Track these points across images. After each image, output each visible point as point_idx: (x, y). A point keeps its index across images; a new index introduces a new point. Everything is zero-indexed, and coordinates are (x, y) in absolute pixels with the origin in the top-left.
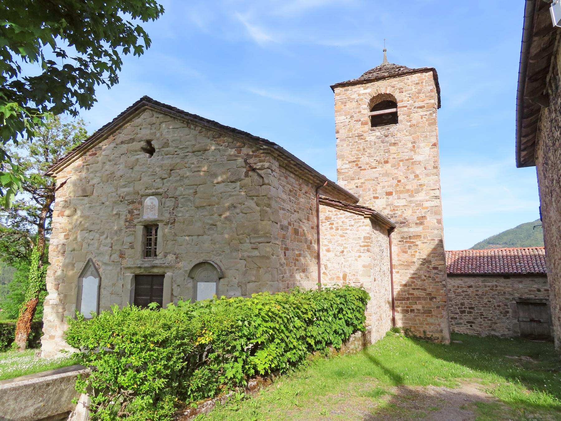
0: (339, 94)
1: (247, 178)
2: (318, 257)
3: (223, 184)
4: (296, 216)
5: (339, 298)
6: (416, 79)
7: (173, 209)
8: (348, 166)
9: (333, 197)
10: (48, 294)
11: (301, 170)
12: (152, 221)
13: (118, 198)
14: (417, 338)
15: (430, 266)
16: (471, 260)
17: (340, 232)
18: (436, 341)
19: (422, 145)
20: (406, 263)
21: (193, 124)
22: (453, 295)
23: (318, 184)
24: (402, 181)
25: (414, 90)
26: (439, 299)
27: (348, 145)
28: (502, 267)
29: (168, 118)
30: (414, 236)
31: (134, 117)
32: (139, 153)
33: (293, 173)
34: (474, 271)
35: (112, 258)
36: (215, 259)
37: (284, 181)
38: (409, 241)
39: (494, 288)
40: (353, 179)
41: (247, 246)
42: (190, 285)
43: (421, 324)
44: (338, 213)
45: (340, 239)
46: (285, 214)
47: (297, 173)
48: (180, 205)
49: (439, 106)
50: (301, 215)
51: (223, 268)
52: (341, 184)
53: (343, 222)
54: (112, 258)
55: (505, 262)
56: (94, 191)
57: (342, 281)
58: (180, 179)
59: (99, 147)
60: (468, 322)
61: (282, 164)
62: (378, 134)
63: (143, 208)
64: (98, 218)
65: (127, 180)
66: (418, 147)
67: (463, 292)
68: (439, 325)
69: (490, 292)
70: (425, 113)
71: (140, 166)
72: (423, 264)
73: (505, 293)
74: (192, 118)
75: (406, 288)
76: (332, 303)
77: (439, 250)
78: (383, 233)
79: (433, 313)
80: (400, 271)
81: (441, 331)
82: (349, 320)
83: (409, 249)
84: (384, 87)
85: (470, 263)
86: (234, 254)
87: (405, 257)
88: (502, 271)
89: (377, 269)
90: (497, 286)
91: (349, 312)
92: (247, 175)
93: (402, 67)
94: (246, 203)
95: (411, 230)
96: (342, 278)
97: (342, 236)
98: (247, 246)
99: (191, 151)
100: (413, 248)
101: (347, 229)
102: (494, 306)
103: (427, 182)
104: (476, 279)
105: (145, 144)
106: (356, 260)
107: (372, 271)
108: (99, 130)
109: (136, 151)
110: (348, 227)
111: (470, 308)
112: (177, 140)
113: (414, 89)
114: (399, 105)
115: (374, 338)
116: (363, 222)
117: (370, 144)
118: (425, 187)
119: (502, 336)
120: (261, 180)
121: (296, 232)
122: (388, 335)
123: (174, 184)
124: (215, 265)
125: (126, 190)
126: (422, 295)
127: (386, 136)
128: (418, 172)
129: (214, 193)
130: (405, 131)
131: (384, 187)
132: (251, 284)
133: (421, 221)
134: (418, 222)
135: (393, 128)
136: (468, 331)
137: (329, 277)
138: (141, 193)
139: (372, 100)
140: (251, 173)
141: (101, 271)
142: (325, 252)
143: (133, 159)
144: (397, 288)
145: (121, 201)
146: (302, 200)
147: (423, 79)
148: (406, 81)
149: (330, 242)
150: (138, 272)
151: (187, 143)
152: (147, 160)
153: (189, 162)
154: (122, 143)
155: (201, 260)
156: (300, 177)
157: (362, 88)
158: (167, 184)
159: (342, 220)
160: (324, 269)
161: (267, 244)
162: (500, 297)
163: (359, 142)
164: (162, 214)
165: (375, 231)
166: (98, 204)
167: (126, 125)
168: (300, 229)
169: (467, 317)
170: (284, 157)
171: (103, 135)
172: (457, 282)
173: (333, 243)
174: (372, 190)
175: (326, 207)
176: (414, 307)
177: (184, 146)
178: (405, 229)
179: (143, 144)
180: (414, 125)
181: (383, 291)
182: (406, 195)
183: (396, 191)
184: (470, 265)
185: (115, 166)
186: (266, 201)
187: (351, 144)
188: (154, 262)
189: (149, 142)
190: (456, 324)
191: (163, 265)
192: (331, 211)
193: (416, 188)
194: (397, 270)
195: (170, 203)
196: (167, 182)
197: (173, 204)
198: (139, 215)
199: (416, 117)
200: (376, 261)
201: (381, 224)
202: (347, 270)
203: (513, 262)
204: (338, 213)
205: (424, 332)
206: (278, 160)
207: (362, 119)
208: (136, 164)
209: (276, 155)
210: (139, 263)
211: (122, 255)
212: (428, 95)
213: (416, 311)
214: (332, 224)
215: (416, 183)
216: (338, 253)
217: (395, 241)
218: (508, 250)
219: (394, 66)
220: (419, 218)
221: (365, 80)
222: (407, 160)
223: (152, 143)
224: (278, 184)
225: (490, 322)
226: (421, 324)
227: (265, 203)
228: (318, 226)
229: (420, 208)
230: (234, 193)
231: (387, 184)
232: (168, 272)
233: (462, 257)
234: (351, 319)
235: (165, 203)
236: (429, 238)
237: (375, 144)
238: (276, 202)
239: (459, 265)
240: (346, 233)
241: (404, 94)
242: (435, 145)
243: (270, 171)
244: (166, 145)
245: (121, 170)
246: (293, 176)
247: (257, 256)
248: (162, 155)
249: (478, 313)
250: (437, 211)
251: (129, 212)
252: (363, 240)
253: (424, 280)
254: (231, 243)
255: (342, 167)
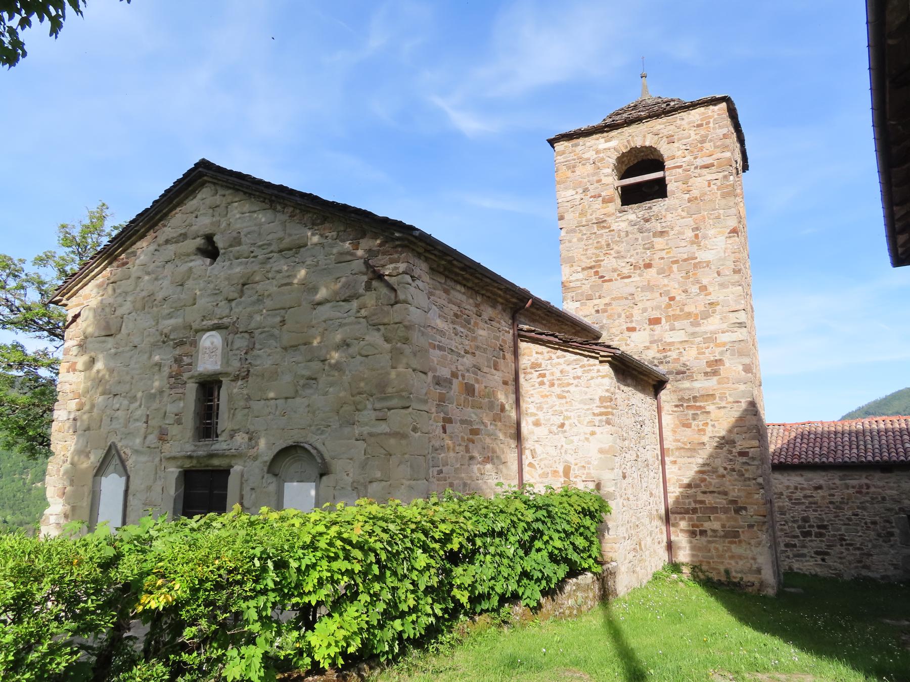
0: (563, 153)
1: (368, 293)
2: (518, 436)
3: (328, 305)
4: (468, 360)
5: (533, 510)
6: (698, 117)
7: (246, 353)
8: (580, 276)
9: (550, 329)
10: (48, 505)
11: (477, 278)
12: (210, 376)
13: (159, 338)
14: (713, 583)
15: (734, 450)
16: (818, 440)
17: (557, 390)
18: (750, 589)
19: (711, 232)
20: (689, 446)
21: (280, 203)
22: (787, 503)
23: (515, 304)
24: (678, 298)
25: (693, 137)
26: (751, 510)
27: (580, 240)
28: (877, 451)
29: (241, 195)
30: (703, 396)
31: (186, 197)
32: (193, 257)
33: (460, 283)
34: (824, 460)
35: (147, 442)
36: (314, 440)
37: (441, 297)
38: (692, 405)
39: (864, 490)
40: (589, 298)
41: (368, 415)
42: (272, 488)
43: (720, 556)
44: (554, 356)
45: (558, 402)
46: (443, 357)
47: (470, 284)
48: (257, 346)
49: (745, 168)
50: (481, 359)
51: (327, 456)
52: (570, 307)
53: (561, 372)
54: (147, 442)
55: (884, 442)
56: (123, 326)
57: (562, 480)
58: (258, 300)
59: (133, 252)
60: (817, 553)
61: (435, 266)
62: (632, 217)
63: (197, 352)
64: (127, 373)
65: (174, 305)
66: (705, 237)
67: (805, 497)
68: (754, 559)
69: (856, 498)
70: (715, 176)
71: (195, 279)
72: (720, 446)
73: (884, 499)
74: (276, 192)
75: (691, 491)
76: (515, 519)
77: (751, 420)
78: (643, 390)
79: (742, 537)
80: (679, 460)
81: (759, 571)
82: (556, 552)
83: (694, 419)
84: (639, 136)
85: (817, 444)
86: (347, 430)
87: (688, 435)
88: (877, 458)
89: (631, 456)
90: (868, 487)
91: (556, 536)
92: (368, 288)
93: (673, 100)
94: (367, 338)
95: (697, 385)
96: (561, 474)
97: (561, 397)
98: (368, 415)
99: (277, 249)
100: (701, 417)
101: (569, 384)
102: (866, 523)
103: (722, 298)
104: (830, 474)
105: (203, 241)
106: (587, 439)
107: (617, 459)
108: (131, 222)
109: (188, 255)
110: (572, 381)
111: (819, 527)
112: (254, 232)
113: (694, 136)
114: (668, 164)
115: (623, 584)
116: (598, 371)
117: (619, 236)
118: (718, 308)
119: (883, 578)
120: (393, 296)
121: (469, 390)
122: (656, 577)
123: (249, 309)
124: (312, 451)
125: (172, 322)
126: (720, 503)
127: (647, 220)
128: (705, 282)
129: (314, 322)
130: (680, 210)
131: (645, 310)
132: (374, 485)
133: (714, 368)
134: (709, 370)
135: (658, 206)
136: (818, 570)
137: (540, 471)
138: (195, 326)
139: (620, 160)
140: (375, 283)
141: (129, 464)
142: (531, 427)
143: (184, 268)
144: (675, 492)
145: (164, 342)
146: (481, 332)
147: (710, 117)
148: (679, 122)
149: (540, 408)
150: (188, 464)
151: (270, 237)
152: (206, 270)
153: (274, 269)
154: (167, 242)
155: (290, 442)
156: (477, 292)
157: (602, 140)
158: (237, 310)
159: (560, 367)
160: (530, 457)
161: (402, 411)
162: (876, 506)
163: (598, 232)
164: (227, 363)
165: (626, 389)
166: (128, 348)
167: (174, 212)
168: (477, 386)
169: (814, 544)
170: (436, 252)
171: (138, 231)
172: (794, 479)
173: (545, 410)
174: (623, 316)
175: (530, 345)
176: (707, 525)
177: (265, 242)
178: (686, 384)
179: (199, 242)
180: (696, 198)
181: (644, 497)
182: (686, 323)
183: (668, 318)
184: (817, 449)
185: (156, 282)
186: (401, 333)
187: (585, 237)
188: (213, 447)
189: (209, 238)
190: (795, 556)
191: (227, 453)
192: (541, 353)
193: (703, 309)
194: (672, 459)
195: (241, 342)
196: (237, 305)
197: (246, 344)
198: (190, 364)
199: (699, 184)
200: (626, 442)
201: (627, 370)
202: (571, 459)
203: (898, 442)
204: (554, 356)
205: (727, 572)
206: (427, 260)
207: (603, 194)
208: (189, 277)
209: (421, 250)
210: (189, 448)
211: (163, 436)
212: (719, 143)
213: (709, 533)
214: (544, 376)
215: (702, 300)
216: (554, 428)
217: (667, 407)
218: (888, 421)
219: (660, 100)
220: (709, 364)
221: (606, 126)
222: (685, 260)
223: (215, 239)
224: (425, 302)
225: (858, 552)
226: (720, 556)
227: (400, 336)
228: (517, 379)
229: (712, 345)
230: (346, 321)
231: (651, 304)
232: (236, 464)
233: (802, 435)
234: (560, 550)
235: (232, 342)
236: (730, 399)
237: (627, 236)
238: (423, 334)
239: (797, 449)
240: (568, 392)
241: (676, 145)
242: (734, 231)
243: (408, 278)
244: (237, 242)
245: (165, 288)
246: (463, 290)
247: (385, 434)
248: (229, 260)
249: (834, 536)
250: (744, 349)
251: (176, 360)
252: (598, 403)
253: (724, 476)
254: (341, 412)
255: (571, 278)
